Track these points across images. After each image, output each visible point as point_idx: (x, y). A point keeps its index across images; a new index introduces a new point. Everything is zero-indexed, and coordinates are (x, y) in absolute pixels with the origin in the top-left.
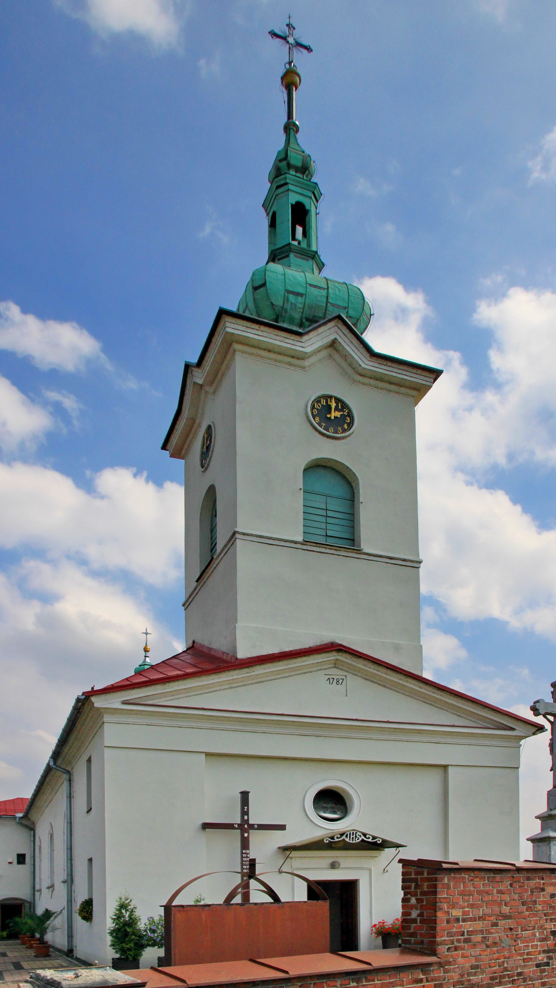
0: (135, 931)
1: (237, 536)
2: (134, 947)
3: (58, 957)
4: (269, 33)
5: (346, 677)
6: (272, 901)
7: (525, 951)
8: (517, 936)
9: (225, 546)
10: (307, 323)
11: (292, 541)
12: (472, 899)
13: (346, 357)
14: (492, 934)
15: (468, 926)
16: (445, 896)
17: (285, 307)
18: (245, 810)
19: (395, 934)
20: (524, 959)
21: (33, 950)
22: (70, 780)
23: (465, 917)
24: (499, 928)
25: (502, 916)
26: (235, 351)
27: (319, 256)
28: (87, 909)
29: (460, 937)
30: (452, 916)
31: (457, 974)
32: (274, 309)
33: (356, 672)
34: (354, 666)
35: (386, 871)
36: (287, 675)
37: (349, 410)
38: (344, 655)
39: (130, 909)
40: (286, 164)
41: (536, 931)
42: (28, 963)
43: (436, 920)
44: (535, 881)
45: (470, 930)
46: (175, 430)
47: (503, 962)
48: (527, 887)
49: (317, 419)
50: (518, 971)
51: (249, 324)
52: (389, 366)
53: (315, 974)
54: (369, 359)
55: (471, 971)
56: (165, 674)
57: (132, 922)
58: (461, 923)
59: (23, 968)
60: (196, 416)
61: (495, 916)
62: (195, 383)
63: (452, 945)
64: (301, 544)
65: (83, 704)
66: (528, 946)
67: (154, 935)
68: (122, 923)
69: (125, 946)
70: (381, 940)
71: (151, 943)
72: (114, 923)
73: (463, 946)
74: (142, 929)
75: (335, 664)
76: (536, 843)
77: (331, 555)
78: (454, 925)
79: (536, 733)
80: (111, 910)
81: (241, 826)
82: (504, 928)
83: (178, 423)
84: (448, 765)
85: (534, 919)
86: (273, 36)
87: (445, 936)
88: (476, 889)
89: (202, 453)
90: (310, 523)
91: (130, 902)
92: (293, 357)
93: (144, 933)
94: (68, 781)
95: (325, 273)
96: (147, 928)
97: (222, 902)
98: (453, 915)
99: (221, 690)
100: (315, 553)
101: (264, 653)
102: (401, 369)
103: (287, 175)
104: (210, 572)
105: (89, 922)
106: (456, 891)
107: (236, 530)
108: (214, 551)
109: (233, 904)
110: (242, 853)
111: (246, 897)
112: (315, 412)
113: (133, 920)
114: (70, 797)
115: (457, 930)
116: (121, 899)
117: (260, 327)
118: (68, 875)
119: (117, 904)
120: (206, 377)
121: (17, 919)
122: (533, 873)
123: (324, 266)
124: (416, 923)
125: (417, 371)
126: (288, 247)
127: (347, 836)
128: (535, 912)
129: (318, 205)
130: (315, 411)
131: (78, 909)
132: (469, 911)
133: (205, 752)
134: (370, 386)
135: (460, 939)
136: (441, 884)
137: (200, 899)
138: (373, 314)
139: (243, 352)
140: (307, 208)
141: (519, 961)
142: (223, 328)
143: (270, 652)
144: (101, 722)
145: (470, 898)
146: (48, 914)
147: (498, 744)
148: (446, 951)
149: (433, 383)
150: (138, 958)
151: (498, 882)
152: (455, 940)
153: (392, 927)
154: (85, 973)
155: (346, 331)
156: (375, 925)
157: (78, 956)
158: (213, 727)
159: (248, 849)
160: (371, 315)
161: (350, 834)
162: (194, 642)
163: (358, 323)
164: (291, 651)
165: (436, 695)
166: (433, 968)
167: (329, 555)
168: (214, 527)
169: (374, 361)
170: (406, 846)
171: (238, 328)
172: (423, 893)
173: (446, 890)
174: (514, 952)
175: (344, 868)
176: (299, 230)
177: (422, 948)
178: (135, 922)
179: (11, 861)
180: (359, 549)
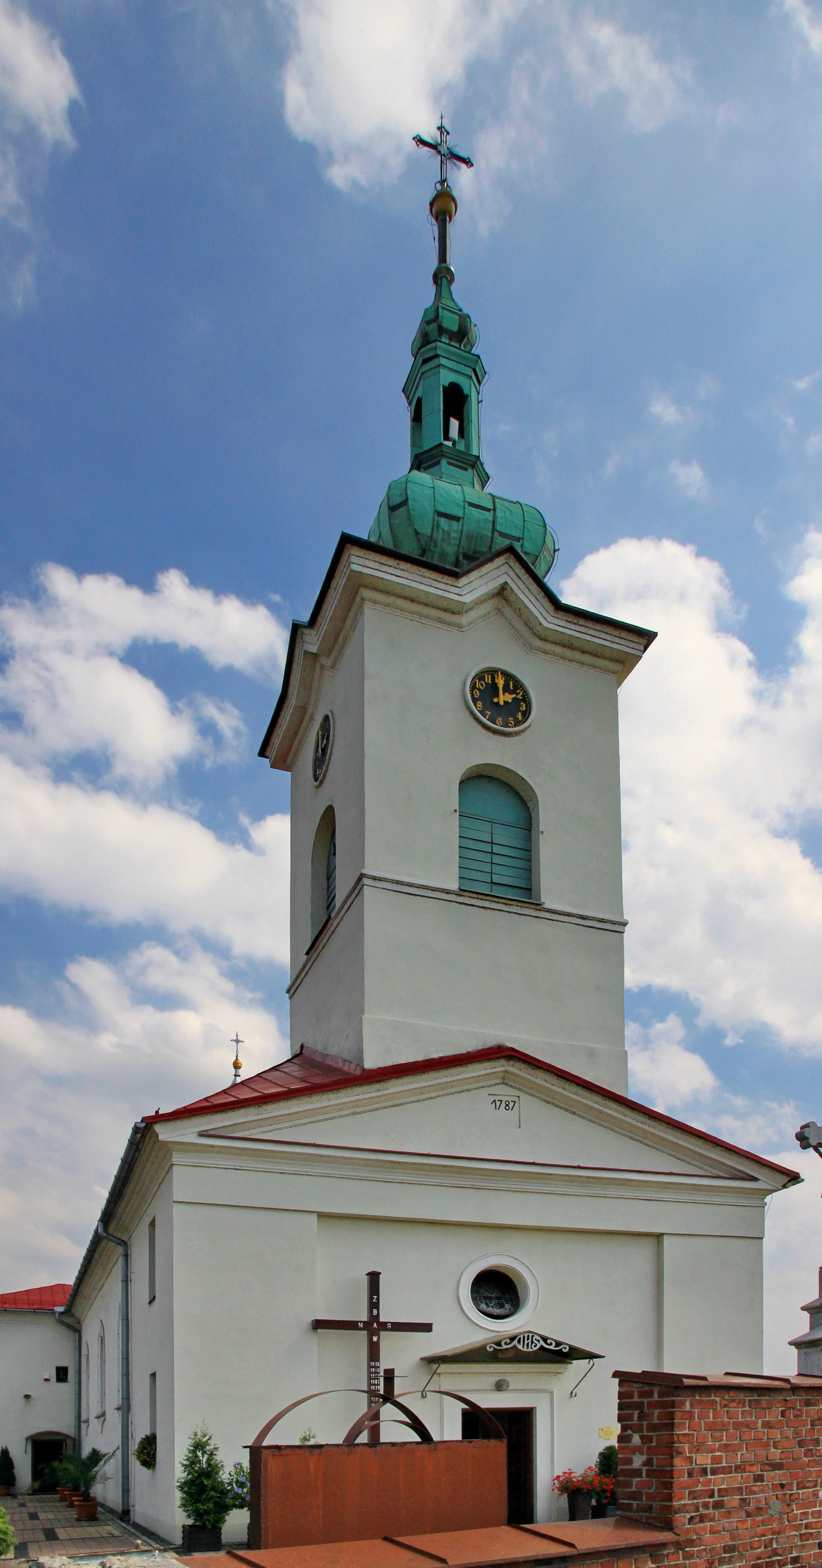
0: (215, 1484)
1: (366, 881)
2: (214, 1510)
3: (108, 1522)
4: (414, 139)
5: (519, 1099)
6: (419, 1440)
7: (802, 1522)
8: (792, 1497)
9: (348, 897)
10: (466, 562)
11: (442, 889)
12: (726, 1436)
13: (520, 611)
14: (755, 1494)
15: (720, 1482)
16: (687, 1431)
17: (434, 537)
18: (374, 1301)
19: (587, 1490)
20: (801, 1535)
21: (75, 1509)
22: (126, 1256)
23: (715, 1466)
24: (764, 1483)
25: (769, 1465)
26: (363, 600)
27: (482, 464)
28: (149, 1450)
29: (707, 1500)
30: (696, 1464)
31: (703, 1560)
32: (418, 540)
33: (533, 1091)
34: (530, 1081)
35: (574, 1394)
36: (433, 1095)
37: (525, 692)
38: (517, 1064)
39: (209, 1451)
40: (436, 327)
41: (819, 1488)
42: (66, 1531)
43: (672, 1471)
44: (817, 1408)
45: (722, 1487)
46: (278, 725)
47: (772, 1539)
48: (806, 1416)
49: (479, 704)
50: (792, 1555)
51: (384, 559)
52: (581, 625)
53: (488, 1564)
54: (553, 614)
55: (724, 1555)
56: (261, 1092)
57: (211, 1471)
58: (709, 1477)
59: (58, 1539)
60: (307, 703)
61: (759, 1464)
62: (306, 653)
63: (696, 1512)
64: (456, 895)
65: (143, 1137)
66: (806, 1514)
67: (243, 1491)
68: (196, 1472)
69: (201, 1507)
70: (567, 1500)
71: (237, 1503)
72: (185, 1472)
73: (712, 1514)
74: (226, 1481)
75: (504, 1079)
76: (802, 1348)
77: (498, 912)
78: (699, 1480)
79: (787, 1186)
80: (181, 1452)
81: (367, 1325)
82: (773, 1484)
83: (282, 714)
84: (663, 1234)
85: (815, 1469)
86: (418, 143)
87: (685, 1498)
88: (732, 1421)
89: (316, 758)
90: (468, 864)
91: (209, 1439)
92: (445, 610)
93: (229, 1488)
94: (124, 1257)
95: (490, 488)
96: (233, 1479)
97: (340, 1442)
98: (698, 1463)
99: (340, 1117)
100: (476, 908)
101: (402, 1060)
102: (599, 631)
103: (439, 344)
104: (325, 939)
105: (151, 1470)
106: (703, 1425)
107: (363, 872)
108: (332, 907)
109: (358, 1445)
110: (370, 1367)
111: (375, 1432)
112: (477, 694)
113: (213, 1467)
114: (126, 1280)
115: (703, 1488)
116: (196, 1434)
117: (398, 564)
118: (123, 1398)
119: (190, 1442)
120: (321, 642)
121: (56, 1464)
122: (815, 1395)
123: (489, 478)
124: (640, 1476)
125: (620, 634)
126: (438, 450)
127: (519, 1341)
128: (817, 1458)
129: (481, 389)
130: (476, 692)
131: (136, 1449)
132: (721, 1456)
133: (317, 1212)
134: (555, 656)
135: (709, 1502)
136: (680, 1411)
137: (309, 1435)
138: (558, 550)
139: (375, 602)
140: (466, 392)
141: (794, 1539)
142: (347, 565)
143: (411, 1060)
144: (169, 1164)
145: (723, 1436)
146: (96, 1457)
147: (733, 1201)
148: (687, 1523)
149: (644, 653)
150: (219, 1525)
151: (764, 1408)
152: (700, 1505)
153: (582, 1480)
154: (118, 1562)
155: (521, 572)
156: (558, 1477)
157: (137, 1521)
158: (328, 1174)
159: (379, 1361)
160: (555, 551)
161: (524, 1337)
162: (302, 1047)
163: (536, 563)
164: (441, 1058)
165: (646, 1127)
166: (668, 1551)
167: (496, 912)
168: (332, 873)
169: (560, 617)
170: (604, 1357)
171: (368, 565)
172: (653, 1428)
173: (687, 1421)
174: (787, 1523)
175: (514, 1390)
176: (454, 424)
177: (647, 1518)
178: (215, 1471)
179: (48, 1377)
180: (539, 903)
